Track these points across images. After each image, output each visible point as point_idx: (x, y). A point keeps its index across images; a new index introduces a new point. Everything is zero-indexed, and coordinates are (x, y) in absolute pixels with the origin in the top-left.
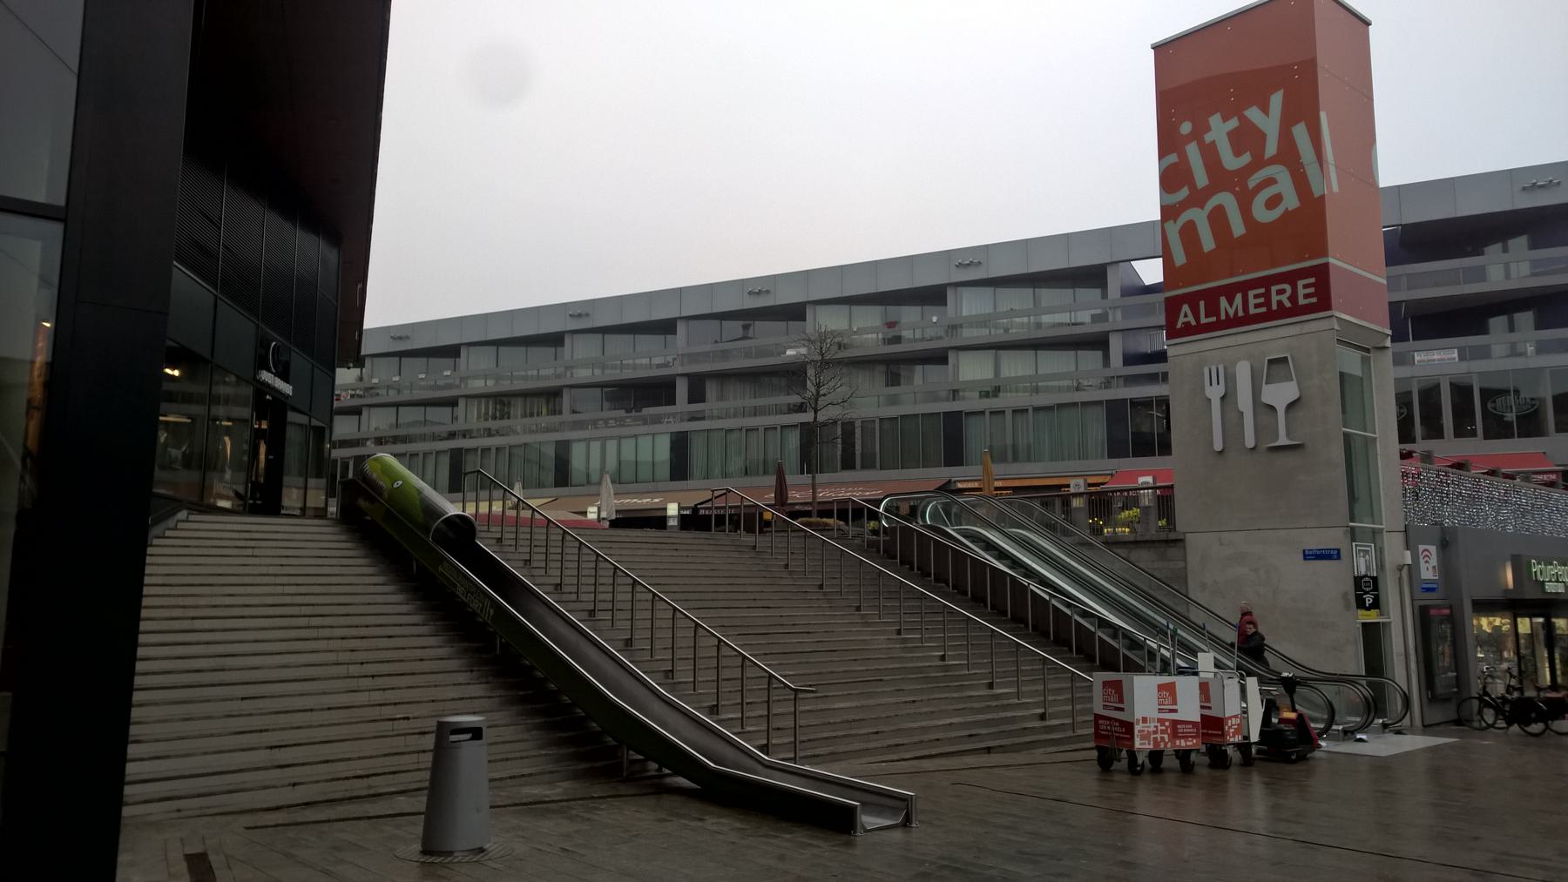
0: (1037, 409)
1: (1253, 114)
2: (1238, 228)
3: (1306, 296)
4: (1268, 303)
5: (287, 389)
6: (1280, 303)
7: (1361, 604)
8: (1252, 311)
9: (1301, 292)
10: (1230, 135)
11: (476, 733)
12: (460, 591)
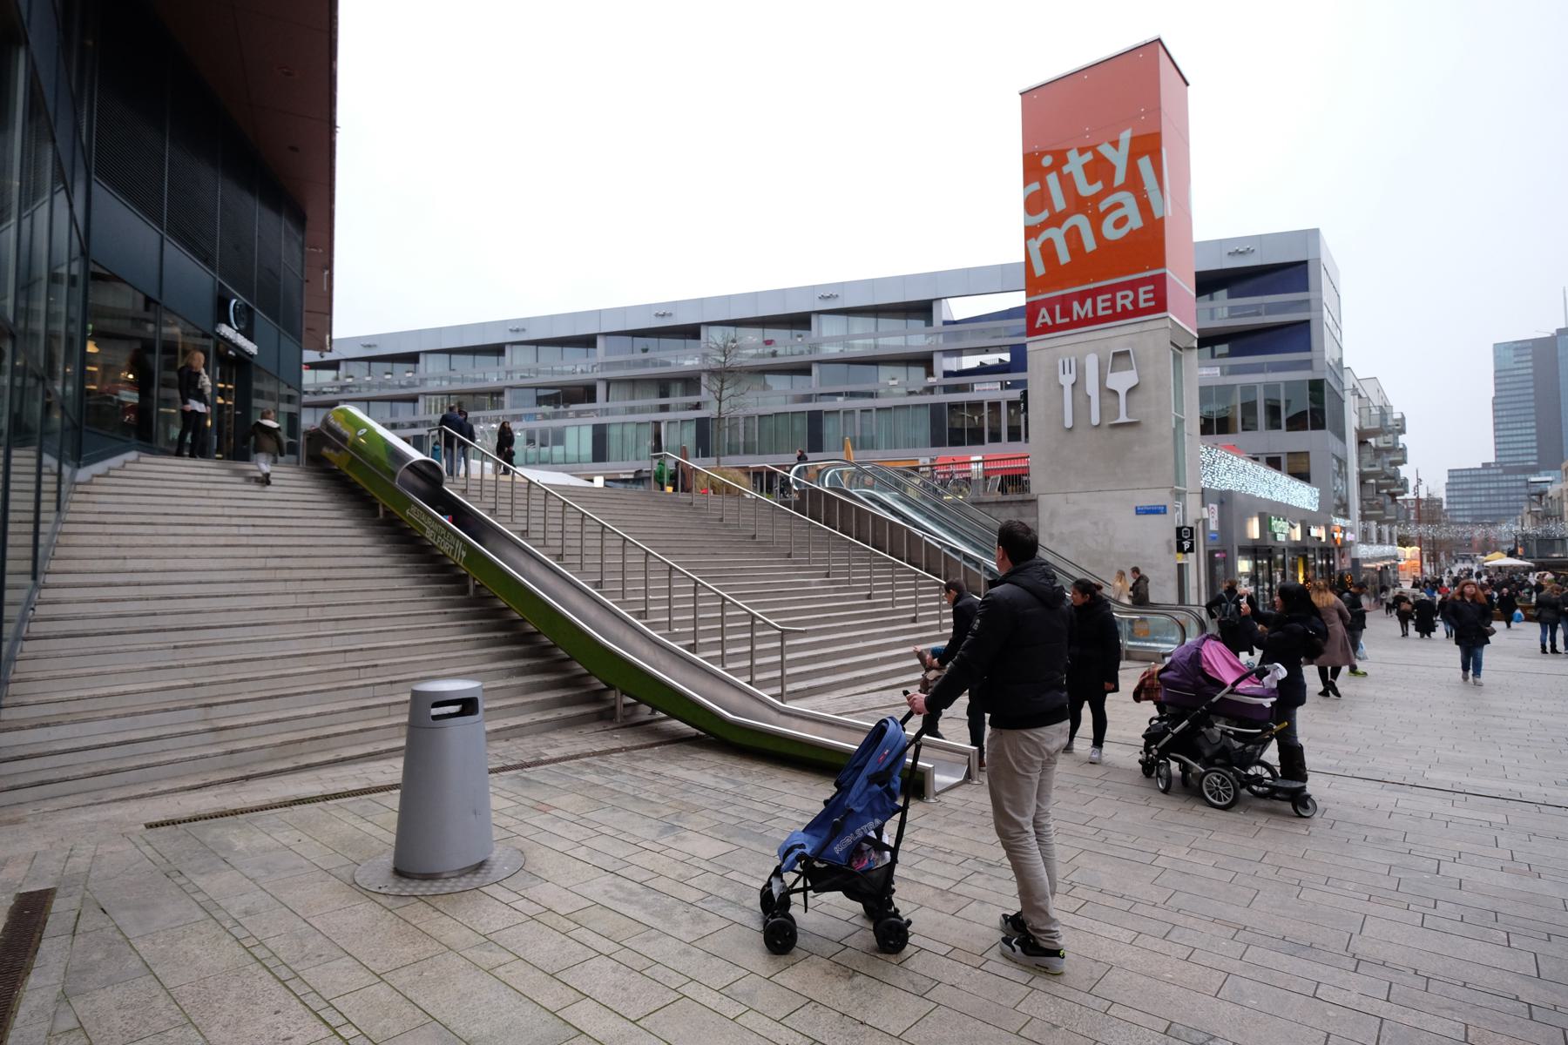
0: (878, 409)
1: (1106, 150)
2: (1090, 244)
3: (1146, 301)
4: (1113, 306)
5: (251, 348)
6: (1124, 306)
7: (1180, 549)
8: (1100, 313)
9: (1142, 297)
10: (1086, 167)
11: (468, 706)
12: (429, 534)
